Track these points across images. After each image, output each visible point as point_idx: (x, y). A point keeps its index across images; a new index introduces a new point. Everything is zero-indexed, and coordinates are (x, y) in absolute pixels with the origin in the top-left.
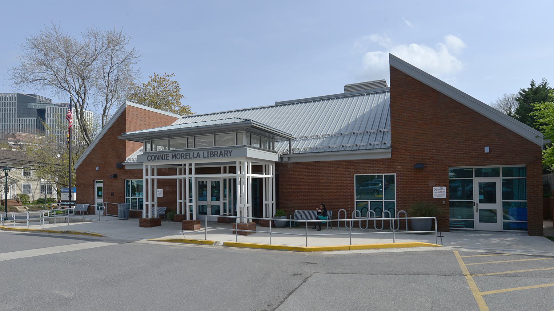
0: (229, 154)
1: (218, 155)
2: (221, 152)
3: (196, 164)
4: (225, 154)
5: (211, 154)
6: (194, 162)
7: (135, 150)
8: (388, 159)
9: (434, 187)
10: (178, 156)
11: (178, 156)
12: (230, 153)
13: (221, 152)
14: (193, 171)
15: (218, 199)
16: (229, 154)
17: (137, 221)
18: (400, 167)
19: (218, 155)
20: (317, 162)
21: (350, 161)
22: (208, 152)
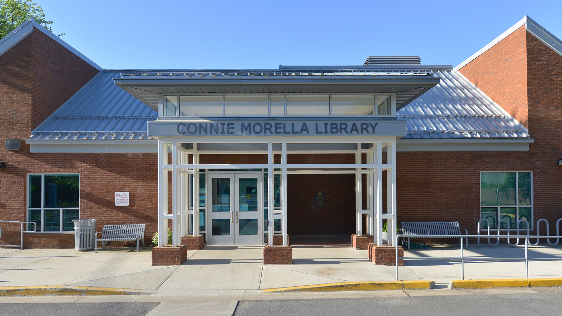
0: (370, 129)
1: (349, 129)
2: (354, 125)
3: (290, 146)
4: (362, 129)
5: (332, 128)
6: (284, 141)
7: (45, 118)
8: (525, 152)
9: (116, 193)
10: (258, 128)
11: (258, 128)
12: (373, 128)
13: (354, 125)
14: (284, 159)
15: (253, 207)
16: (370, 129)
17: (148, 255)
18: (539, 163)
19: (349, 129)
20: (428, 152)
21: (476, 152)
22: (326, 124)
